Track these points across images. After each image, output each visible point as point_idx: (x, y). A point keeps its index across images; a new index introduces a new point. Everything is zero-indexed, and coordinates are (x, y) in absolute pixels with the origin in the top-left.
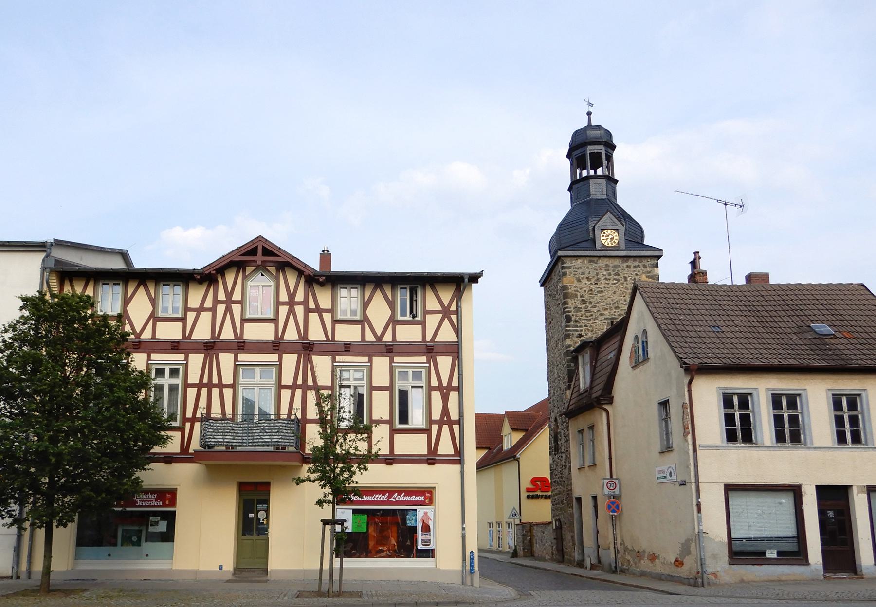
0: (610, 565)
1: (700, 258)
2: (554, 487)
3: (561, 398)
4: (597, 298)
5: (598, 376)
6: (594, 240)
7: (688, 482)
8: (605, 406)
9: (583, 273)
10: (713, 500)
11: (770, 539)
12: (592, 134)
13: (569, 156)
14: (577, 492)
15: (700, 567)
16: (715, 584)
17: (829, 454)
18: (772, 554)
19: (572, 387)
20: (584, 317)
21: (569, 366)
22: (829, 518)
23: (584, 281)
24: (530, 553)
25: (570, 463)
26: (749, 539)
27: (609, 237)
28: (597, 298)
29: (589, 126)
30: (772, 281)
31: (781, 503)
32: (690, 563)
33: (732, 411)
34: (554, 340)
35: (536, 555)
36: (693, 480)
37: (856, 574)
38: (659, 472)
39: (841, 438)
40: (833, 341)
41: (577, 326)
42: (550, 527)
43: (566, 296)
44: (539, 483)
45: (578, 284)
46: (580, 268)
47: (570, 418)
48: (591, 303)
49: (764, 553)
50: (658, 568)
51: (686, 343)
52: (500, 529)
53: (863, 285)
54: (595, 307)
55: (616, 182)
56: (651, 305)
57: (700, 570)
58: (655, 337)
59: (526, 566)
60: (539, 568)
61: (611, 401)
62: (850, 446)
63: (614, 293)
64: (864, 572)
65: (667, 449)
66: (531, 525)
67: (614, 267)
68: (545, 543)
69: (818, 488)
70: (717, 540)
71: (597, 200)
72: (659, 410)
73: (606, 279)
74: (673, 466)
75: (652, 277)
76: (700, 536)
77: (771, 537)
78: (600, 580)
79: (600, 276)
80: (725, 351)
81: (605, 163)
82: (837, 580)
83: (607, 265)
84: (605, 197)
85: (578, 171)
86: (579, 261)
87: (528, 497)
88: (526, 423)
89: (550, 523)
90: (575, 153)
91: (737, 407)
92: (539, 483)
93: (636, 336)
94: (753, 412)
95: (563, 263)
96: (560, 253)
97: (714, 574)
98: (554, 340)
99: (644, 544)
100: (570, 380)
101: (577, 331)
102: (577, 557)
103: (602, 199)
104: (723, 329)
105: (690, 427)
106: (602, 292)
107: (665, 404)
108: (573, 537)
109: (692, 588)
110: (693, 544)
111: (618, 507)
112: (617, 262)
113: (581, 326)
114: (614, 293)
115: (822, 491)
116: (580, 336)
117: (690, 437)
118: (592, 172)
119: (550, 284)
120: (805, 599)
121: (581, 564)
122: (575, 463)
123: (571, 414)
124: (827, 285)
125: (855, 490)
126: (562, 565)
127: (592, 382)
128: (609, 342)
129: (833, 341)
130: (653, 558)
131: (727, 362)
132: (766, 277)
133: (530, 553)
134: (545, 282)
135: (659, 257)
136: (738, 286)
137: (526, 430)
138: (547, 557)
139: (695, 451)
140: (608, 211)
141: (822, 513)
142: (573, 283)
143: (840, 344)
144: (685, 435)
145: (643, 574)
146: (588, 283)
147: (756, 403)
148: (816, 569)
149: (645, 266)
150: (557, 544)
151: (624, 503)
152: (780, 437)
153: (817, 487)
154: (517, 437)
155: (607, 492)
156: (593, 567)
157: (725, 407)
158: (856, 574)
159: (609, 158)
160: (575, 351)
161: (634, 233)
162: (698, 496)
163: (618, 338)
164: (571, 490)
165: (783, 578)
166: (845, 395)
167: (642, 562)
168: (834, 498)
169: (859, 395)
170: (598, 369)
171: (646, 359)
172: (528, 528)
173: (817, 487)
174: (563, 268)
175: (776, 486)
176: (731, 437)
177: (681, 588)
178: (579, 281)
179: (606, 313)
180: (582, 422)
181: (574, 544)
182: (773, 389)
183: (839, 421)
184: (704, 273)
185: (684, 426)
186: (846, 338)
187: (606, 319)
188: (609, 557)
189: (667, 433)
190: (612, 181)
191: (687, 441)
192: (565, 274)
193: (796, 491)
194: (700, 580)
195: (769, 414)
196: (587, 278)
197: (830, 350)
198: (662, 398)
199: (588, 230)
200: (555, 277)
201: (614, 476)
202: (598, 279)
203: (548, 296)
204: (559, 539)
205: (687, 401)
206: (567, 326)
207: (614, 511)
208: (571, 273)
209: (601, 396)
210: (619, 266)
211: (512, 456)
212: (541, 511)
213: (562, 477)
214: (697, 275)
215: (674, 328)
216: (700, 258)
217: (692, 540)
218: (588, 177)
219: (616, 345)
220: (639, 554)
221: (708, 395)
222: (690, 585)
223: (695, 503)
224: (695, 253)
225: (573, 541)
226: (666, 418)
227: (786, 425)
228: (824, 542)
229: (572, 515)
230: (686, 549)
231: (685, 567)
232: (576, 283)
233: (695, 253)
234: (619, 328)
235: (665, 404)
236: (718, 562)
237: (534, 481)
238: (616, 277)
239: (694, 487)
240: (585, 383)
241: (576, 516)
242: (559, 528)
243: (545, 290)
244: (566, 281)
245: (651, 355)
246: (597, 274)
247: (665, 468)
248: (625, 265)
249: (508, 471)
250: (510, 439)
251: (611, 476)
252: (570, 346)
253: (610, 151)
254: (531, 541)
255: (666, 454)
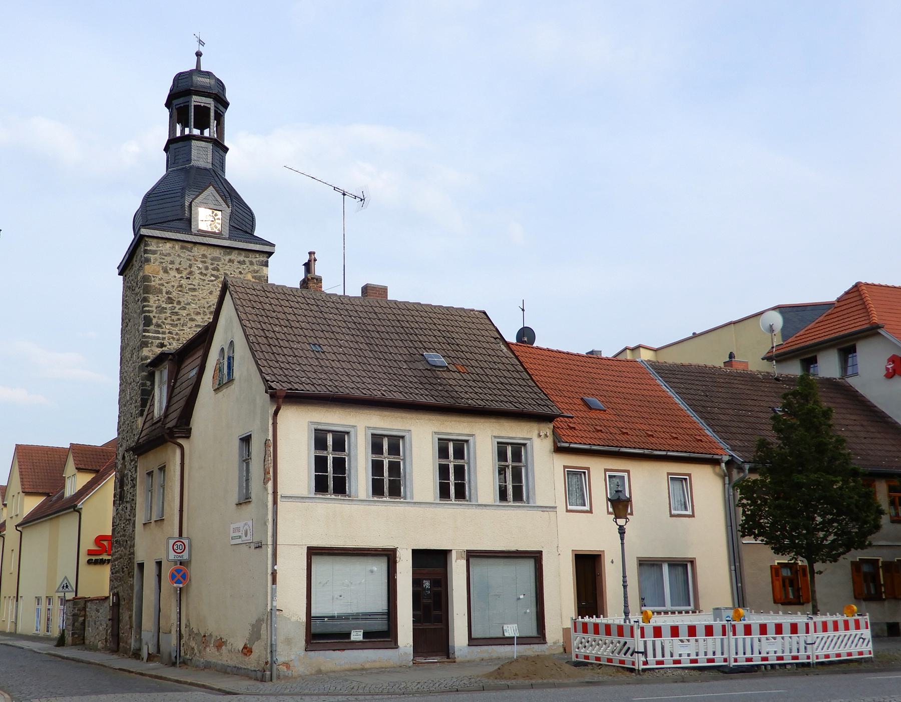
0: (170, 655)
1: (315, 260)
2: (115, 550)
3: (131, 426)
4: (187, 298)
5: (175, 400)
6: (189, 221)
7: (265, 545)
8: (180, 441)
9: (172, 263)
10: (291, 566)
11: (356, 617)
12: (200, 80)
13: (168, 104)
14: (141, 555)
15: (269, 656)
16: (286, 677)
17: (429, 511)
18: (357, 636)
19: (145, 413)
20: (168, 321)
21: (143, 385)
22: (424, 589)
23: (173, 273)
24: (80, 640)
25: (135, 516)
26: (332, 618)
27: (208, 218)
28: (187, 298)
29: (198, 71)
30: (391, 296)
31: (372, 572)
32: (258, 649)
33: (324, 454)
34: (129, 349)
35: (87, 642)
36: (270, 541)
37: (448, 657)
38: (235, 530)
39: (444, 492)
40: (445, 375)
41: (158, 332)
42: (106, 604)
43: (147, 290)
44: (105, 543)
45: (165, 276)
46: (169, 255)
47: (139, 455)
48: (179, 303)
49: (348, 635)
50: (225, 658)
51: (277, 362)
52: (50, 607)
53: (485, 313)
54: (184, 308)
55: (226, 150)
56: (241, 309)
57: (269, 659)
58: (242, 352)
59: (67, 658)
60: (82, 662)
61: (187, 434)
62: (453, 502)
63: (211, 293)
64: (457, 654)
65: (245, 500)
66: (87, 600)
67: (213, 259)
68: (98, 628)
69: (416, 553)
70: (294, 619)
71: (198, 168)
72: (241, 449)
73: (201, 273)
74: (250, 523)
75: (259, 278)
76: (273, 613)
77: (358, 614)
78: (151, 676)
79: (194, 269)
80: (323, 376)
81: (213, 123)
82: (426, 666)
83: (204, 256)
84: (209, 166)
85: (179, 127)
86: (168, 245)
87: (90, 562)
88: (92, 460)
89: (107, 598)
90: (175, 102)
91: (330, 448)
92: (105, 543)
93: (222, 349)
94: (349, 455)
95: (146, 245)
96: (144, 231)
97: (287, 665)
98: (129, 349)
99: (212, 627)
100: (144, 403)
101: (158, 338)
102: (133, 644)
103: (206, 169)
104: (325, 348)
105: (272, 474)
106: (194, 290)
107: (246, 440)
108: (130, 617)
109: (259, 684)
110: (264, 625)
111: (184, 577)
112: (217, 253)
113: (164, 333)
114: (211, 293)
115: (419, 555)
116: (162, 345)
117: (270, 485)
118: (196, 132)
119: (130, 273)
120: (382, 693)
121: (137, 655)
122: (140, 517)
123: (141, 449)
124: (448, 308)
125: (454, 554)
126: (115, 656)
127: (168, 407)
128: (192, 356)
129: (445, 375)
130: (220, 644)
131: (322, 390)
132: (383, 291)
133: (80, 640)
134: (124, 269)
135: (270, 254)
136: (350, 298)
137: (97, 471)
138: (100, 645)
139: (275, 502)
140: (210, 184)
141: (417, 583)
142: (158, 273)
143: (452, 379)
144: (265, 482)
145: (208, 666)
146: (178, 276)
147: (352, 445)
148: (406, 653)
149: (251, 263)
150: (112, 626)
151: (194, 571)
152: (377, 489)
153: (414, 551)
154: (83, 479)
155: (172, 555)
156: (150, 658)
157: (316, 448)
158: (448, 657)
159: (219, 118)
160: (150, 364)
161: (241, 220)
162: (275, 562)
163: (200, 353)
164: (133, 553)
165: (367, 666)
166: (453, 440)
167: (208, 649)
168: (431, 564)
169: (467, 441)
170: (177, 391)
171: (231, 380)
172: (81, 605)
173: (414, 551)
174: (146, 252)
175: (369, 549)
176: (321, 486)
177: (242, 685)
178: (166, 271)
179: (198, 318)
180: (150, 461)
181: (131, 627)
182: (374, 428)
183: (443, 471)
184: (319, 280)
185: (265, 470)
186: (459, 372)
187: (196, 326)
188: (170, 642)
189: (247, 479)
190: (220, 147)
191: (266, 489)
192: (147, 260)
193: (390, 556)
194: (268, 673)
195: (367, 459)
196: (177, 269)
197: (441, 385)
198: (243, 433)
199: (183, 206)
200: (136, 264)
201: (185, 535)
202: (191, 273)
203: (128, 288)
204: (115, 620)
205: (270, 437)
206: (145, 331)
207: (178, 582)
208: (156, 260)
209: (175, 427)
210: (219, 259)
211: (72, 506)
212: (98, 582)
213: (124, 536)
214: (310, 280)
215: (265, 341)
216: (315, 260)
217: (263, 620)
218: (191, 137)
219: (198, 361)
220: (205, 639)
221: (296, 429)
222: (256, 679)
223: (270, 571)
224: (310, 253)
225: (131, 622)
226: (246, 460)
227: (386, 473)
228: (416, 620)
229: (132, 587)
230: (256, 634)
231: (254, 656)
232: (161, 274)
233: (310, 253)
234: (206, 336)
235: (246, 440)
236: (291, 650)
237: (99, 540)
238: (215, 273)
239: (270, 550)
240: (160, 409)
241: (136, 588)
242: (116, 606)
243: (124, 280)
244: (148, 269)
245: (236, 374)
246: (190, 266)
247: (240, 524)
248: (227, 258)
249: (66, 526)
250: (75, 481)
251: (181, 534)
252: (146, 358)
253: (221, 108)
254: (83, 623)
255: (244, 507)
